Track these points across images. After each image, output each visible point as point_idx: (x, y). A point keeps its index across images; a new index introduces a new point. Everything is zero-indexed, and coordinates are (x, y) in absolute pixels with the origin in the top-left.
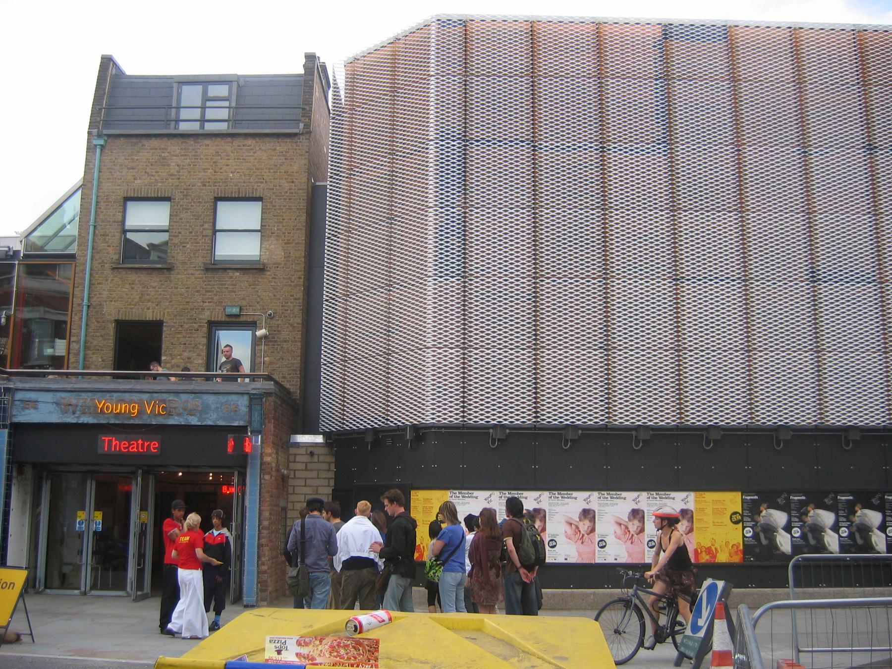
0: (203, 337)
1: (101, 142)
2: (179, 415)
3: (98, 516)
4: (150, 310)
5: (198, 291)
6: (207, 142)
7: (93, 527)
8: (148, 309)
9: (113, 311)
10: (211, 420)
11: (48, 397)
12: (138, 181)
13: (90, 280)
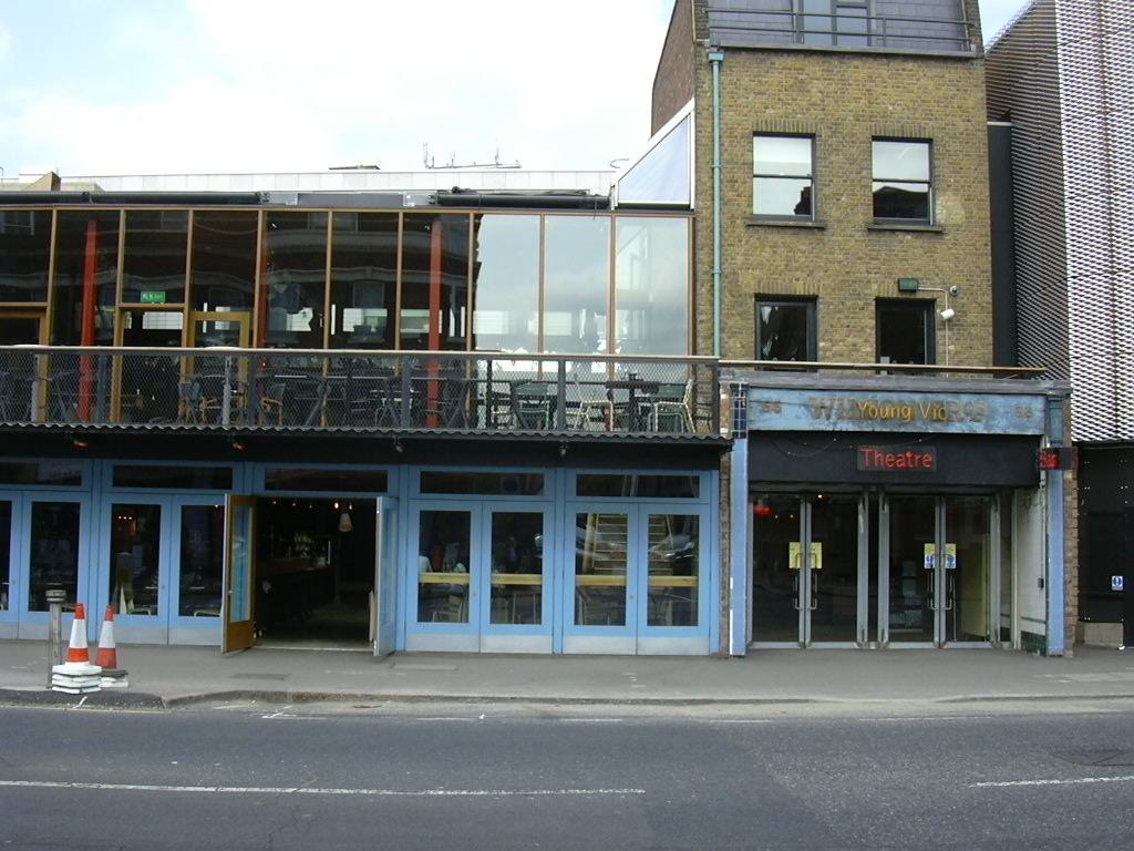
0: (871, 318)
1: (720, 57)
2: (961, 420)
3: (817, 548)
4: (801, 282)
5: (860, 258)
6: (856, 62)
7: (946, 564)
8: (798, 280)
9: (750, 282)
10: (1000, 426)
11: (793, 397)
12: (770, 111)
13: (720, 241)
